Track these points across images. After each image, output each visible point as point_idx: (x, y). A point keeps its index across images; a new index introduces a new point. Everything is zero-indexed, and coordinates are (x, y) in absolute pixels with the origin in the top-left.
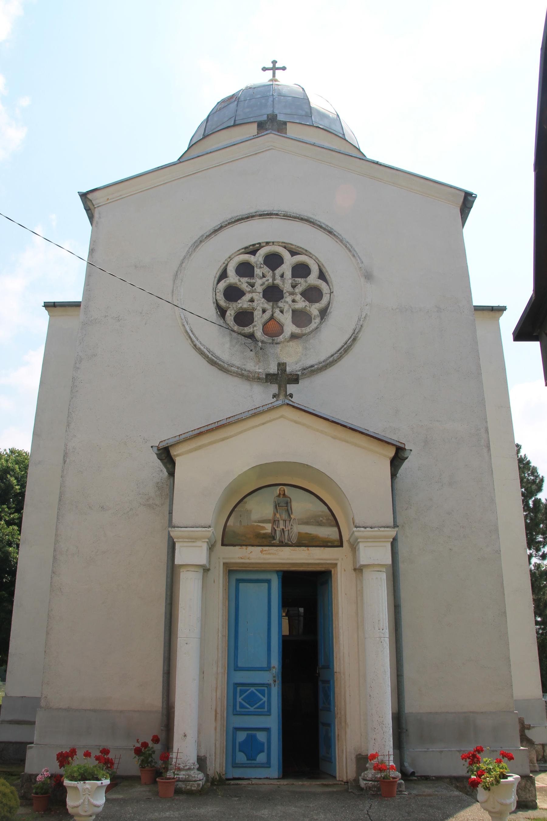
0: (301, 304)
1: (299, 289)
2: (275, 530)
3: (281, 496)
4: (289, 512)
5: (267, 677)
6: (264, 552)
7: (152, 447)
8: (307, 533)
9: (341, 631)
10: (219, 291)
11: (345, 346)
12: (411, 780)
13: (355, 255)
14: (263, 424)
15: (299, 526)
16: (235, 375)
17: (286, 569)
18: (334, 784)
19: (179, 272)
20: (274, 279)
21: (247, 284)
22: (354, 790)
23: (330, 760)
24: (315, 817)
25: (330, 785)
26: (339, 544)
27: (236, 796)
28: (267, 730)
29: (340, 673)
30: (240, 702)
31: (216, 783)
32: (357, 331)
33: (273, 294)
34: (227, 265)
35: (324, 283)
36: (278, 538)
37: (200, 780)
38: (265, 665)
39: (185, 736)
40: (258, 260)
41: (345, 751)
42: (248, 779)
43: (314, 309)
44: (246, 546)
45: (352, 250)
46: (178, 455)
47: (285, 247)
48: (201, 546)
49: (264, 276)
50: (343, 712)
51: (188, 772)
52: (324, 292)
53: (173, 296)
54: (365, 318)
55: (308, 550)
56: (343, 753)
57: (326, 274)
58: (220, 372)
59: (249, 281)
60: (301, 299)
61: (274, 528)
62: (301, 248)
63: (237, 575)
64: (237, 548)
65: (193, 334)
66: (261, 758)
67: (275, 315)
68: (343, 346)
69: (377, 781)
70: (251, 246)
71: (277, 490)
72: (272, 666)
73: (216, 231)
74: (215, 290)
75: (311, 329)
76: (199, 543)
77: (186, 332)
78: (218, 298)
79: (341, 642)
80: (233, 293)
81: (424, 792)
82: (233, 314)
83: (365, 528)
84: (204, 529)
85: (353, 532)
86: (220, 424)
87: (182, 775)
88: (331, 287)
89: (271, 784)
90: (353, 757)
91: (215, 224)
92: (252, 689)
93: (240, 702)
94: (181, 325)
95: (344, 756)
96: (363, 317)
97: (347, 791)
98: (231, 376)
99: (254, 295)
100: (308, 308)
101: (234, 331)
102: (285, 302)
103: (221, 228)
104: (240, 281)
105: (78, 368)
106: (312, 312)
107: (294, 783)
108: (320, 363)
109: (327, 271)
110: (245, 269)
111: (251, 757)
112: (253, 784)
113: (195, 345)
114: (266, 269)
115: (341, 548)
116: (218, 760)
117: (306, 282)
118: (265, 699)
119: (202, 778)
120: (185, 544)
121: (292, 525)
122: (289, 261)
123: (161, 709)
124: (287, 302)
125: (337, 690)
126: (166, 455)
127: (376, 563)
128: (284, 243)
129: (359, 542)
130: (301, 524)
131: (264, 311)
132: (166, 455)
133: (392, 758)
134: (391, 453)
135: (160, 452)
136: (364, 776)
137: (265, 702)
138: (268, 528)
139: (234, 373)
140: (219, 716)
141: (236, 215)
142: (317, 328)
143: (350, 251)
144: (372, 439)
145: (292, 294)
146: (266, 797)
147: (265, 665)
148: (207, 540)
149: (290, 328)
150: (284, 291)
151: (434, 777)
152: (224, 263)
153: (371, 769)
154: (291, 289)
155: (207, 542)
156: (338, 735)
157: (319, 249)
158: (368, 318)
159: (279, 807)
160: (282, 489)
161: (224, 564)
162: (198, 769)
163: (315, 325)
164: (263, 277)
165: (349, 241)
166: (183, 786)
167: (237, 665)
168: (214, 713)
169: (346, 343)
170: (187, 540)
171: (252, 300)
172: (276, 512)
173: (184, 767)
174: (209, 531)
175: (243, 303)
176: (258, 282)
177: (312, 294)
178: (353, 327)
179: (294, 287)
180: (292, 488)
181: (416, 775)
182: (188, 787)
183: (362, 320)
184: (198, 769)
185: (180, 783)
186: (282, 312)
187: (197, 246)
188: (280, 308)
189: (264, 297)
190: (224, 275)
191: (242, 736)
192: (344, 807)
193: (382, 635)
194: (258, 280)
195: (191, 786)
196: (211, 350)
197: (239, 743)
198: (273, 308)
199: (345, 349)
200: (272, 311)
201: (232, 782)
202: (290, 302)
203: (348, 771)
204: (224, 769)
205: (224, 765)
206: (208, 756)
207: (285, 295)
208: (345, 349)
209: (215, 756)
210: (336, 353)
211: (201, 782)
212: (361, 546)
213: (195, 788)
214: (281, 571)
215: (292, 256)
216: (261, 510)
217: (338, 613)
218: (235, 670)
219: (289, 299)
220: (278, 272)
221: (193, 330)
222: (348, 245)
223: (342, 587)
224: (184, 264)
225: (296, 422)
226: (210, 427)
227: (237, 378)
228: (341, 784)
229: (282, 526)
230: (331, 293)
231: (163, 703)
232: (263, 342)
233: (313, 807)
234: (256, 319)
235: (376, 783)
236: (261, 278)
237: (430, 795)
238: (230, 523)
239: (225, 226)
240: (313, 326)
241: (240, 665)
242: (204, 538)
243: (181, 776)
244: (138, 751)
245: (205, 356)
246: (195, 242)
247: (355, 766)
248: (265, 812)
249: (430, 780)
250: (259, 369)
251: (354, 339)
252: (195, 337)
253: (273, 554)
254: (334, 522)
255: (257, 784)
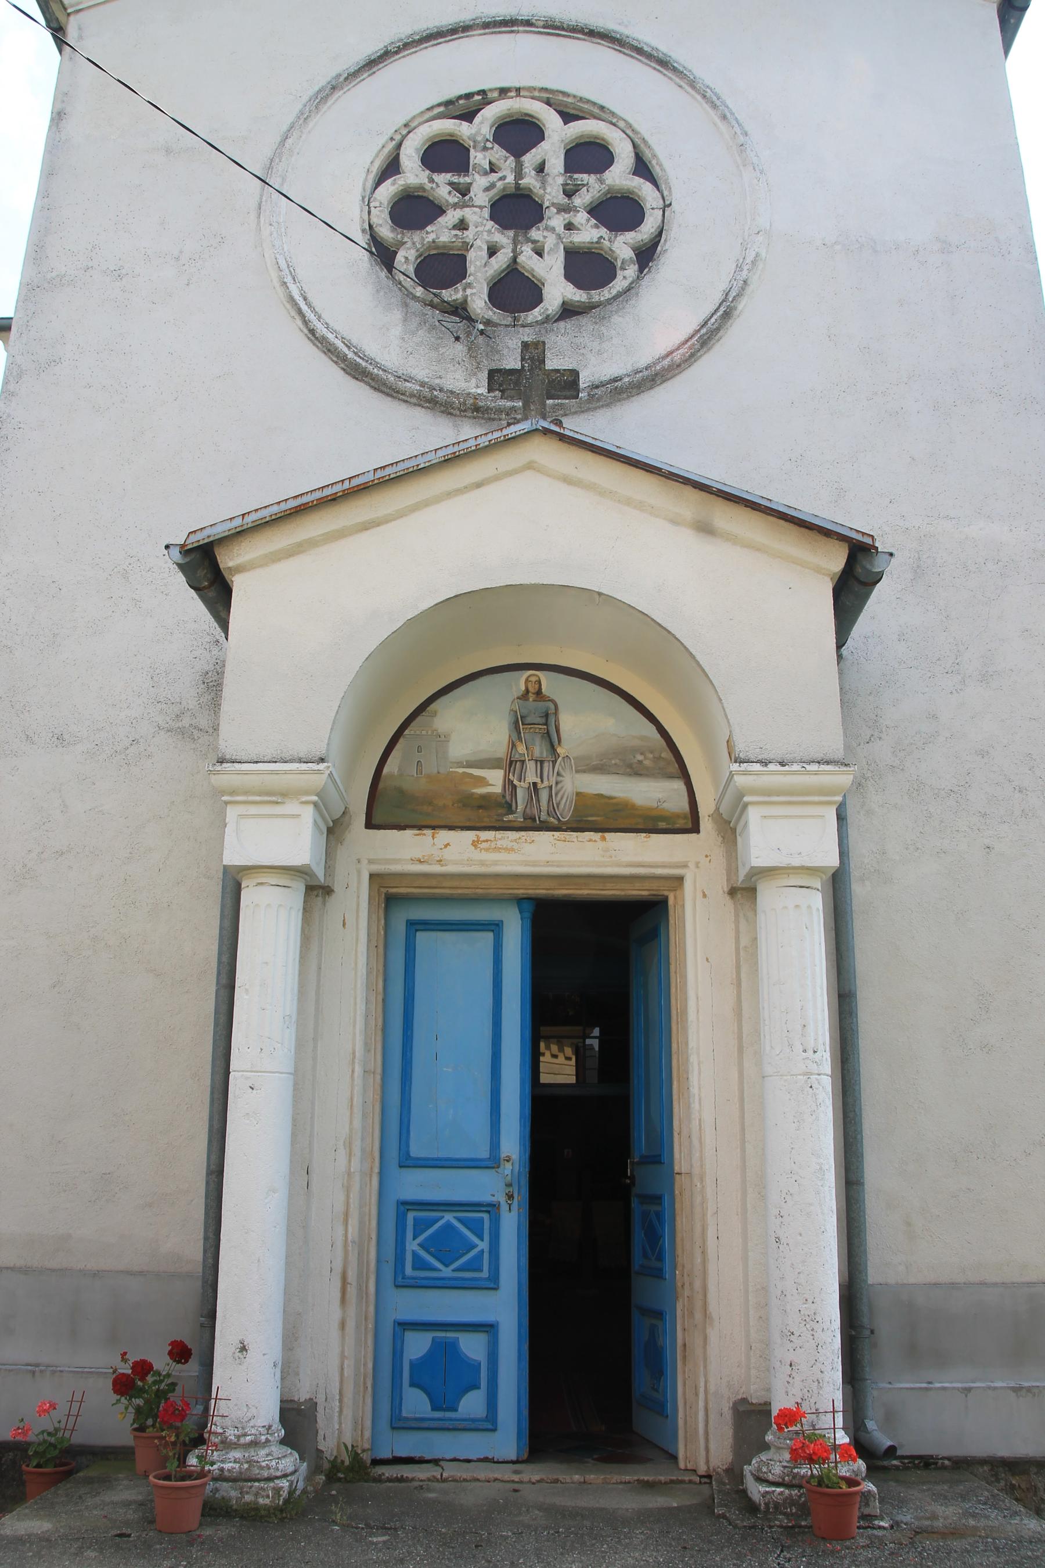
0: (589, 233)
1: (582, 199)
2: (515, 787)
3: (531, 697)
4: (551, 739)
6: (484, 845)
7: (167, 547)
9: (693, 1059)
10: (378, 204)
11: (703, 331)
12: (885, 1469)
13: (728, 115)
14: (479, 485)
15: (578, 776)
17: (541, 892)
18: (672, 1482)
19: (277, 160)
20: (519, 173)
21: (449, 188)
22: (724, 1499)
23: (661, 1407)
25: (660, 1482)
26: (690, 826)
27: (384, 1529)
28: (489, 1328)
29: (689, 1174)
32: (733, 294)
33: (517, 210)
34: (399, 145)
35: (648, 183)
36: (520, 807)
37: (285, 1476)
38: (484, 1153)
39: (243, 1349)
40: (478, 133)
41: (702, 1390)
42: (436, 1462)
43: (622, 247)
44: (434, 828)
45: (718, 103)
46: (239, 569)
47: (548, 103)
49: (493, 169)
50: (698, 1284)
52: (647, 207)
53: (259, 217)
54: (754, 263)
55: (604, 839)
56: (697, 1395)
57: (654, 162)
59: (455, 179)
60: (588, 221)
62: (588, 101)
64: (409, 833)
65: (309, 305)
66: (472, 1404)
67: (521, 259)
68: (699, 330)
69: (800, 1487)
70: (460, 97)
71: (520, 681)
72: (503, 1155)
73: (372, 64)
74: (368, 202)
75: (614, 292)
76: (291, 807)
77: (292, 299)
78: (375, 220)
79: (694, 1090)
80: (413, 210)
81: (934, 1517)
82: (412, 258)
84: (304, 766)
85: (731, 775)
86: (355, 482)
87: (230, 1462)
88: (666, 193)
89: (496, 1480)
90: (727, 1409)
91: (373, 47)
92: (449, 1217)
94: (277, 284)
95: (701, 1404)
96: (748, 260)
97: (708, 1507)
98: (404, 406)
99: (468, 213)
100: (606, 243)
101: (415, 298)
102: (547, 228)
103: (385, 56)
104: (432, 181)
105: (12, 394)
106: (618, 252)
107: (561, 1477)
108: (637, 372)
109: (654, 156)
110: (446, 155)
112: (444, 1480)
113: (312, 332)
114: (498, 153)
116: (348, 1412)
117: (602, 181)
118: (483, 1245)
120: (253, 810)
121: (558, 774)
122: (558, 134)
123: (201, 1270)
124: (553, 230)
125: (681, 1223)
126: (206, 570)
127: (796, 862)
128: (546, 90)
129: (746, 805)
130: (584, 771)
131: (492, 251)
132: (206, 570)
135: (187, 560)
136: (759, 1470)
137: (483, 1251)
138: (494, 781)
139: (412, 395)
140: (352, 1291)
141: (425, 27)
142: (628, 289)
143: (714, 106)
145: (562, 209)
147: (484, 1153)
148: (315, 798)
149: (558, 290)
150: (546, 204)
151: (949, 1459)
152: (392, 139)
154: (562, 199)
155: (315, 804)
156: (685, 1345)
157: (632, 99)
158: (761, 266)
160: (533, 679)
161: (372, 876)
162: (283, 1442)
163: (625, 284)
164: (490, 171)
165: (711, 85)
166: (234, 1494)
167: (408, 1153)
168: (338, 1284)
169: (706, 323)
170: (258, 798)
171: (462, 225)
172: (515, 736)
173: (238, 1437)
175: (440, 232)
176: (479, 182)
177: (619, 211)
178: (723, 286)
179: (569, 194)
180: (562, 676)
181: (899, 1453)
182: (248, 1498)
183: (745, 268)
184: (283, 1442)
185: (225, 1484)
186: (540, 253)
187: (325, 99)
188: (534, 242)
189: (492, 217)
190: (392, 167)
191: (418, 1345)
193: (814, 1068)
194: (477, 176)
195: (257, 1494)
196: (354, 342)
198: (515, 242)
199: (706, 337)
200: (514, 251)
201: (388, 1471)
202: (560, 229)
203: (712, 1446)
204: (368, 1434)
205: (368, 1423)
206: (320, 1399)
207: (547, 214)
208: (706, 337)
209: (341, 1401)
210: (678, 349)
211: (284, 1484)
212: (753, 815)
213: (267, 1501)
214: (529, 899)
215: (565, 124)
216: (474, 734)
217: (685, 1011)
218: (401, 1167)
219: (557, 221)
220: (530, 159)
221: (309, 296)
222: (709, 94)
223: (699, 937)
224: (290, 141)
228: (690, 1482)
229: (531, 777)
230: (666, 206)
231: (205, 1251)
232: (488, 323)
234: (471, 269)
236: (486, 174)
237: (955, 1533)
238: (389, 768)
239: (396, 53)
240: (619, 284)
241: (415, 1151)
242: (307, 793)
243: (227, 1466)
244: (123, 1386)
245: (338, 357)
246: (319, 91)
249: (937, 1469)
250: (477, 387)
251: (725, 314)
252: (314, 311)
254: (674, 767)
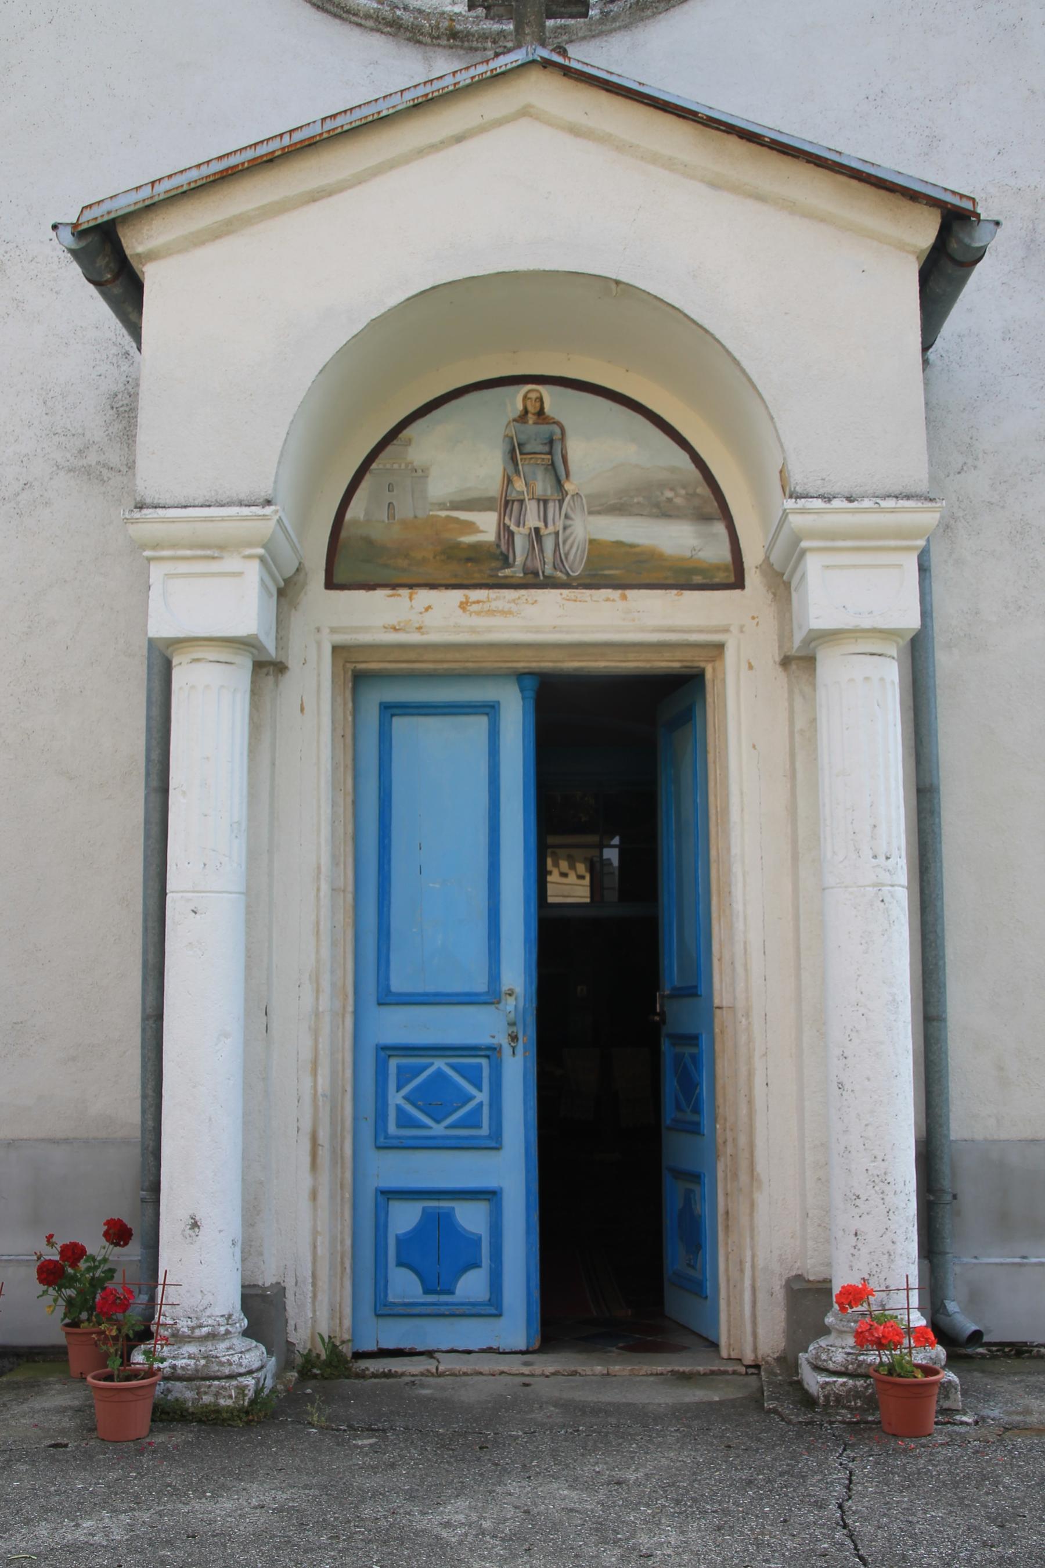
2: (511, 534)
3: (531, 419)
4: (557, 471)
5: (486, 1026)
6: (475, 608)
7: (55, 227)
8: (619, 544)
9: (737, 869)
14: (459, 139)
15: (591, 518)
16: (370, 23)
18: (713, 1373)
22: (779, 1405)
23: (699, 1287)
24: (644, 1540)
25: (698, 1373)
26: (732, 579)
28: (490, 1196)
29: (732, 1008)
30: (399, 1109)
31: (317, 1371)
36: (519, 560)
37: (250, 1372)
38: (480, 985)
39: (195, 1225)
41: (748, 1266)
42: (430, 1354)
44: (411, 586)
46: (151, 256)
48: (240, 574)
50: (743, 1140)
51: (208, 1347)
55: (624, 598)
56: (742, 1271)
58: (319, 15)
61: (507, 528)
63: (378, 688)
64: (380, 594)
66: (472, 1285)
69: (867, 1376)
71: (516, 398)
72: (505, 988)
76: (232, 563)
79: (738, 907)
83: (828, 498)
84: (245, 511)
85: (785, 514)
86: (298, 137)
87: (183, 1358)
89: (502, 1373)
92: (440, 1064)
93: (399, 1109)
95: (747, 1282)
97: (757, 1401)
98: (357, 31)
107: (579, 1369)
111: (437, 1283)
112: (440, 1375)
115: (737, 592)
116: (323, 1298)
118: (482, 1097)
119: (256, 1365)
120: (183, 567)
121: (567, 517)
123: (138, 1134)
125: (723, 1067)
126: (108, 256)
127: (866, 623)
129: (803, 553)
132: (108, 256)
133: (915, 1300)
134: (924, 232)
135: (83, 244)
136: (817, 1357)
137: (481, 1104)
138: (486, 526)
139: (368, 16)
144: (854, 183)
146: (472, 1436)
147: (480, 985)
148: (261, 551)
153: (841, 1332)
155: (262, 559)
156: (727, 1213)
159: (513, 1486)
160: (533, 395)
161: (336, 649)
162: (246, 1333)
166: (189, 1395)
167: (388, 986)
172: (511, 469)
173: (193, 1329)
174: (264, 518)
180: (570, 392)
181: (985, 1339)
182: (207, 1399)
184: (246, 1333)
185: (178, 1384)
191: (405, 1217)
192: (750, 1483)
193: (885, 878)
195: (217, 1395)
197: (399, 1240)
201: (373, 1366)
203: (761, 1331)
204: (347, 1322)
206: (289, 1284)
211: (250, 1381)
212: (813, 564)
213: (230, 1402)
214: (531, 674)
216: (459, 466)
217: (726, 810)
218: (380, 1004)
225: (575, 131)
226: (262, 150)
227: (377, 35)
228: (734, 1373)
229: (533, 520)
233: (637, 1483)
235: (860, 1383)
238: (356, 511)
241: (398, 984)
242: (250, 545)
243: (180, 1363)
244: (50, 1274)
247: (783, 1315)
248: (455, 1515)
249: (1031, 1358)
253: (505, 613)
255: (453, 1374)
